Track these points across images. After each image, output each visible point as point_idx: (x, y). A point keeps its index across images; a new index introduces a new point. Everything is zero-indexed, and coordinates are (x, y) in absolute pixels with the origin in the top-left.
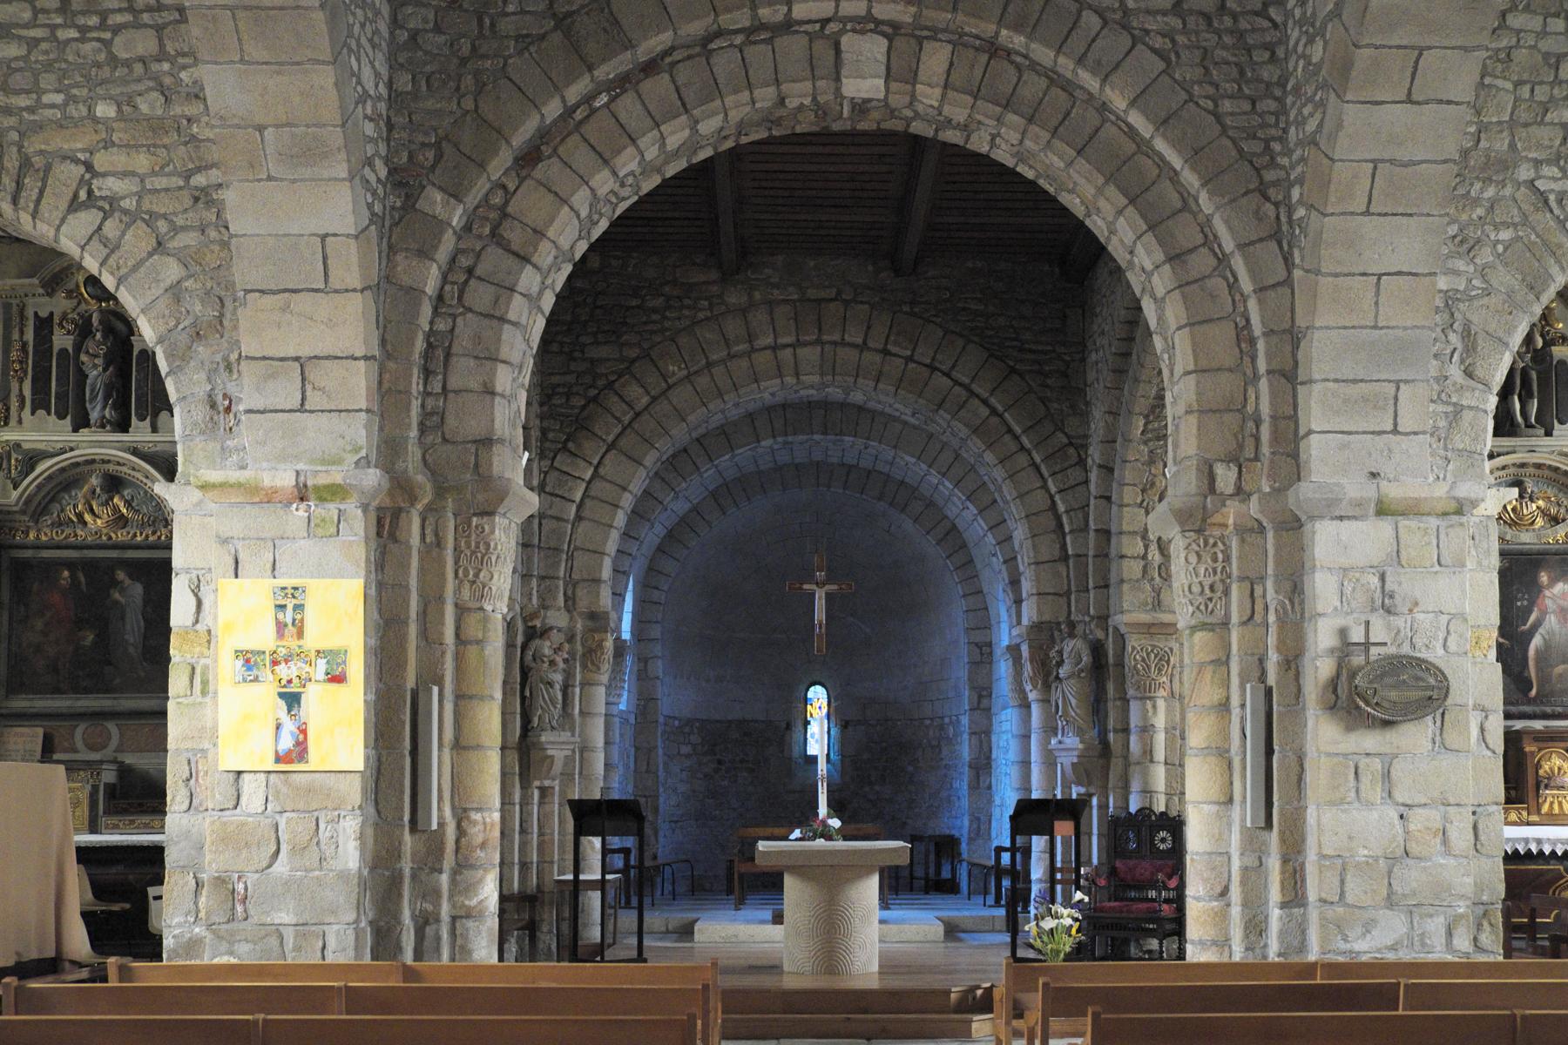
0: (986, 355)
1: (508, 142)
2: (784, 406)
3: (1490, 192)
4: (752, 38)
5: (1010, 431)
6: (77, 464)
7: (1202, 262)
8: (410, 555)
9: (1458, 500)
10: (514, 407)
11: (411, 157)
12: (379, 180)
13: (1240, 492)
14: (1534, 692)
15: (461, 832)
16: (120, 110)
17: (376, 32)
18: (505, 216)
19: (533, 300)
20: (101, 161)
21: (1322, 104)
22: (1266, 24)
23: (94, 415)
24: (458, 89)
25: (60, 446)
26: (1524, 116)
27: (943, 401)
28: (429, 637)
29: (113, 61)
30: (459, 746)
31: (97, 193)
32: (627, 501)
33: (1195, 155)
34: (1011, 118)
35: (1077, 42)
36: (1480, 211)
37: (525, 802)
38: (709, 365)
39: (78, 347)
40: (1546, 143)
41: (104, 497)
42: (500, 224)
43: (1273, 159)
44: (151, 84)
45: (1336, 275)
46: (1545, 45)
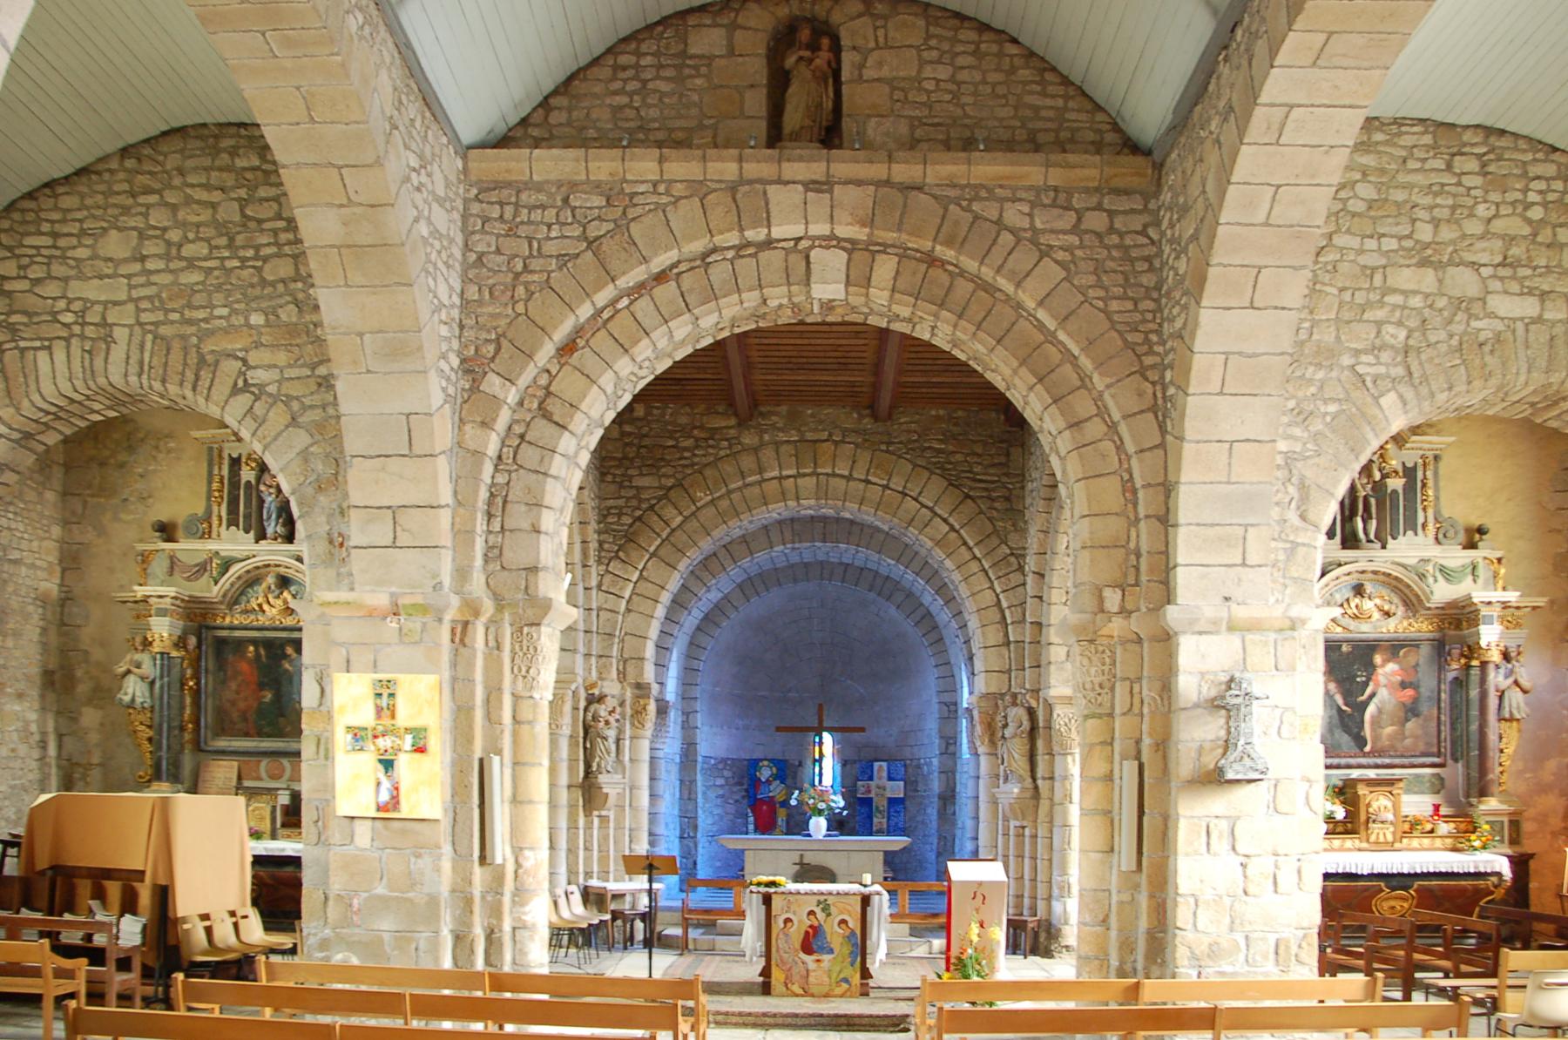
0: (946, 483)
1: (551, 338)
2: (792, 520)
3: (1320, 375)
4: (741, 253)
5: (965, 543)
6: (258, 568)
7: (1095, 429)
8: (475, 656)
9: (1291, 620)
10: (556, 540)
11: (477, 350)
12: (452, 369)
13: (1124, 612)
14: (1367, 749)
15: (518, 865)
16: (267, 320)
17: (451, 256)
18: (549, 394)
19: (571, 459)
20: (253, 358)
21: (1185, 307)
22: (1146, 241)
23: (270, 531)
24: (513, 297)
25: (246, 553)
26: (1347, 315)
27: (912, 520)
28: (491, 718)
29: (264, 283)
30: (516, 800)
31: (250, 382)
32: (666, 597)
33: (1089, 344)
34: (945, 314)
35: (997, 256)
36: (1313, 390)
37: (589, 827)
38: (729, 492)
39: (259, 479)
40: (1365, 336)
41: (277, 592)
42: (544, 400)
43: (1151, 347)
44: (289, 298)
45: (1198, 442)
46: (1362, 260)
